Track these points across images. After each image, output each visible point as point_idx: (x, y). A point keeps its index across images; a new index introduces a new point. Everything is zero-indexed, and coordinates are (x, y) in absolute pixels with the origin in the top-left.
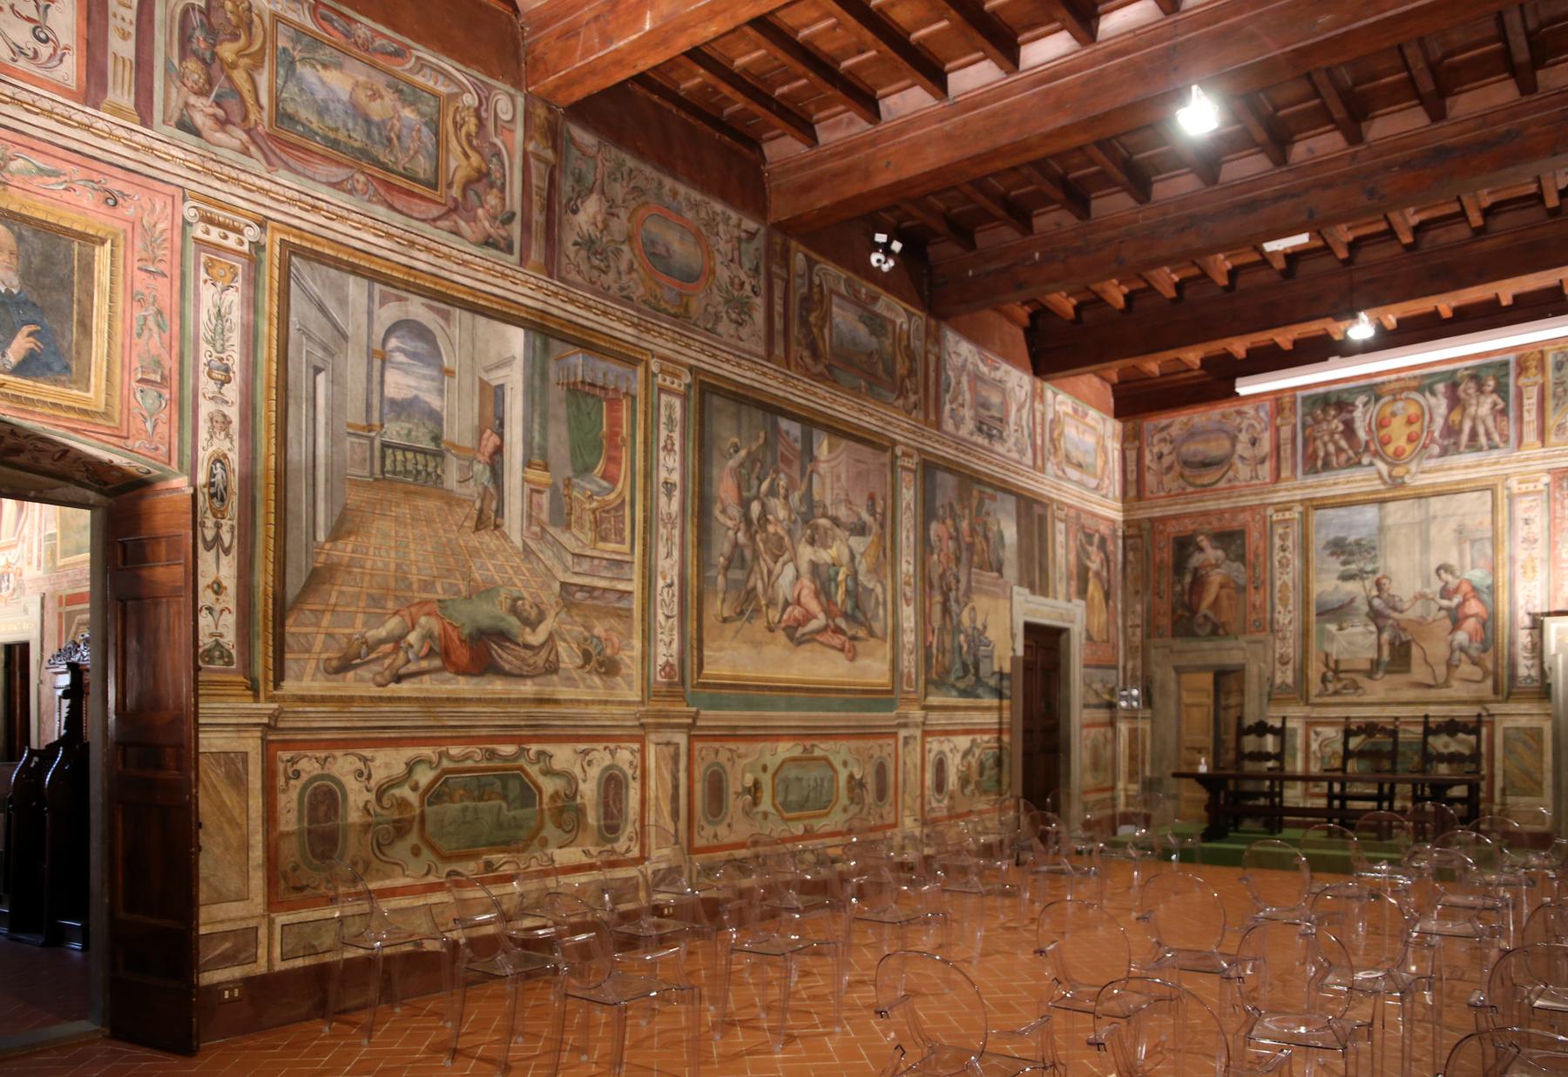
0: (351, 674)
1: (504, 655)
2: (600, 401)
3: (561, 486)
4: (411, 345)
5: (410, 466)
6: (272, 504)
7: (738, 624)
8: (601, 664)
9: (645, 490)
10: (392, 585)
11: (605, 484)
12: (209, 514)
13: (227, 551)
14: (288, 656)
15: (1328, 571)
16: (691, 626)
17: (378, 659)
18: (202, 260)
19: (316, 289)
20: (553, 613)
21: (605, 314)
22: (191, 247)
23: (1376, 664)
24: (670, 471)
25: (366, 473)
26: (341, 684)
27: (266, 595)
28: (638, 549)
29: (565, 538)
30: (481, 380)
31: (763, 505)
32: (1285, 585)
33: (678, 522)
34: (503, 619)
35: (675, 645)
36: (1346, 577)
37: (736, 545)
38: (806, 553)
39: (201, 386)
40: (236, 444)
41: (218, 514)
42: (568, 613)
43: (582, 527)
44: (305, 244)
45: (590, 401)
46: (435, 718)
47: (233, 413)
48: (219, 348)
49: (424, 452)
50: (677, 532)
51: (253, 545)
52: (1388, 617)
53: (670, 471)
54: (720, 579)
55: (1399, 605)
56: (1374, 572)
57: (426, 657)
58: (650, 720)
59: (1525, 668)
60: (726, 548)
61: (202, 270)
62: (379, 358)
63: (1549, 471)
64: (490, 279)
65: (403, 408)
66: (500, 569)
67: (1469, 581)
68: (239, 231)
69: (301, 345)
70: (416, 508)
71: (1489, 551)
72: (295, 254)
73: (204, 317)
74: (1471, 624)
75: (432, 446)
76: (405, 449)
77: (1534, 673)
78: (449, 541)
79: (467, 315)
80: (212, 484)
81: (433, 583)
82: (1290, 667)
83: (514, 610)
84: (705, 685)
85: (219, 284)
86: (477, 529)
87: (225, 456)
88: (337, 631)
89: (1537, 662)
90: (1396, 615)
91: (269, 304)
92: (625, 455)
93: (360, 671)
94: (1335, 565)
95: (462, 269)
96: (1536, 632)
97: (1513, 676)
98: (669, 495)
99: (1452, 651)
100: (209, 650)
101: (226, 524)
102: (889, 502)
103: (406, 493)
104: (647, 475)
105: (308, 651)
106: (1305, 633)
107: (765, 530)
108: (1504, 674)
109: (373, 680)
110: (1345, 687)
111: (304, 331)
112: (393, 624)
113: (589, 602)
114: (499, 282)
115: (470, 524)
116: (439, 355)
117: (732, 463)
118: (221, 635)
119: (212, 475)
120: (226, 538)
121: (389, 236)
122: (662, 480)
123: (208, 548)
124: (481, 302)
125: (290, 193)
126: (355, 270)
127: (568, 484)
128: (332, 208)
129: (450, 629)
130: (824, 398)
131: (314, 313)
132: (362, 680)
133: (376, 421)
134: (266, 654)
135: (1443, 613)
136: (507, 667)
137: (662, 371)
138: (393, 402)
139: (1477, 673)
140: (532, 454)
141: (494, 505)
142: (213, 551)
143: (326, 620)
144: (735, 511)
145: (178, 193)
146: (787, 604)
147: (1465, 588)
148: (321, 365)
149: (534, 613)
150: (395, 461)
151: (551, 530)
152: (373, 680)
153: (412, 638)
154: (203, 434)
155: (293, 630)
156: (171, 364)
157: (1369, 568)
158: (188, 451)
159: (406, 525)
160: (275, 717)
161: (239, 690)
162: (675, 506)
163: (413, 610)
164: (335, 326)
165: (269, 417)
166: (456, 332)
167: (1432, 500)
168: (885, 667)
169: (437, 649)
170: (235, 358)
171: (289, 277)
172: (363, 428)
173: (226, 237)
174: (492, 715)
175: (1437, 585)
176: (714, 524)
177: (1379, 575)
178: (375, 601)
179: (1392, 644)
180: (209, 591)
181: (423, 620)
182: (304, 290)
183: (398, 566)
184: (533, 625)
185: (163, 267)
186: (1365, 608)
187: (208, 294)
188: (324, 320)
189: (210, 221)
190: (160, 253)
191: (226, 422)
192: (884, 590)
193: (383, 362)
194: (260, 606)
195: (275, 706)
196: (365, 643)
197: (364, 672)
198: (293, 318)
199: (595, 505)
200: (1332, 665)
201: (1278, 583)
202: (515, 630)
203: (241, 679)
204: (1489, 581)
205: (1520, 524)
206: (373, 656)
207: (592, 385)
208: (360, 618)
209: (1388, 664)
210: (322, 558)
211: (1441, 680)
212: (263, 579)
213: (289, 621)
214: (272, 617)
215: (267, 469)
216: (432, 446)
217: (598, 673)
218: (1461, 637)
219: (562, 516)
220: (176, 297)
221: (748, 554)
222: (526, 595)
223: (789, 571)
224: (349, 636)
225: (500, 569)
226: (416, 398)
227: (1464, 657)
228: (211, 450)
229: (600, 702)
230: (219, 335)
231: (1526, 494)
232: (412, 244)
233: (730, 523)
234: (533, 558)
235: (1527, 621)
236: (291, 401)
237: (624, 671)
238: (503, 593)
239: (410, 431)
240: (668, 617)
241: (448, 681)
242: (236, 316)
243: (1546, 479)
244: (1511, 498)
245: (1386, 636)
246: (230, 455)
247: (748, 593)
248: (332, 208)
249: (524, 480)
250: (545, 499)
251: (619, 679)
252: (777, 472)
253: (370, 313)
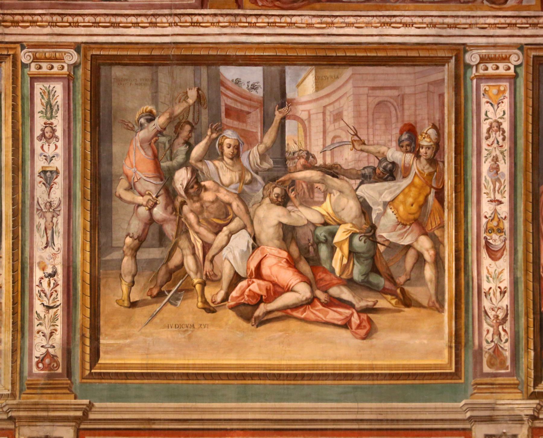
7: (157, 307)
9: (15, 183)
16: (83, 316)
31: (195, 171)
33: (63, 210)
35: (58, 337)
37: (151, 221)
38: (270, 217)
54: (127, 263)
58: (21, 414)
60: (136, 227)
84: (101, 376)
98: (49, 184)
102: (449, 128)
107: (200, 199)
117: (142, 134)
122: (38, 169)
130: (310, 26)
137: (35, 59)
144: (150, 185)
146: (237, 278)
162: (58, 192)
168: (443, 341)
176: (116, 204)
192: (437, 244)
221: (170, 229)
223: (242, 241)
233: (140, 200)
247: (170, 273)
252: (220, 130)
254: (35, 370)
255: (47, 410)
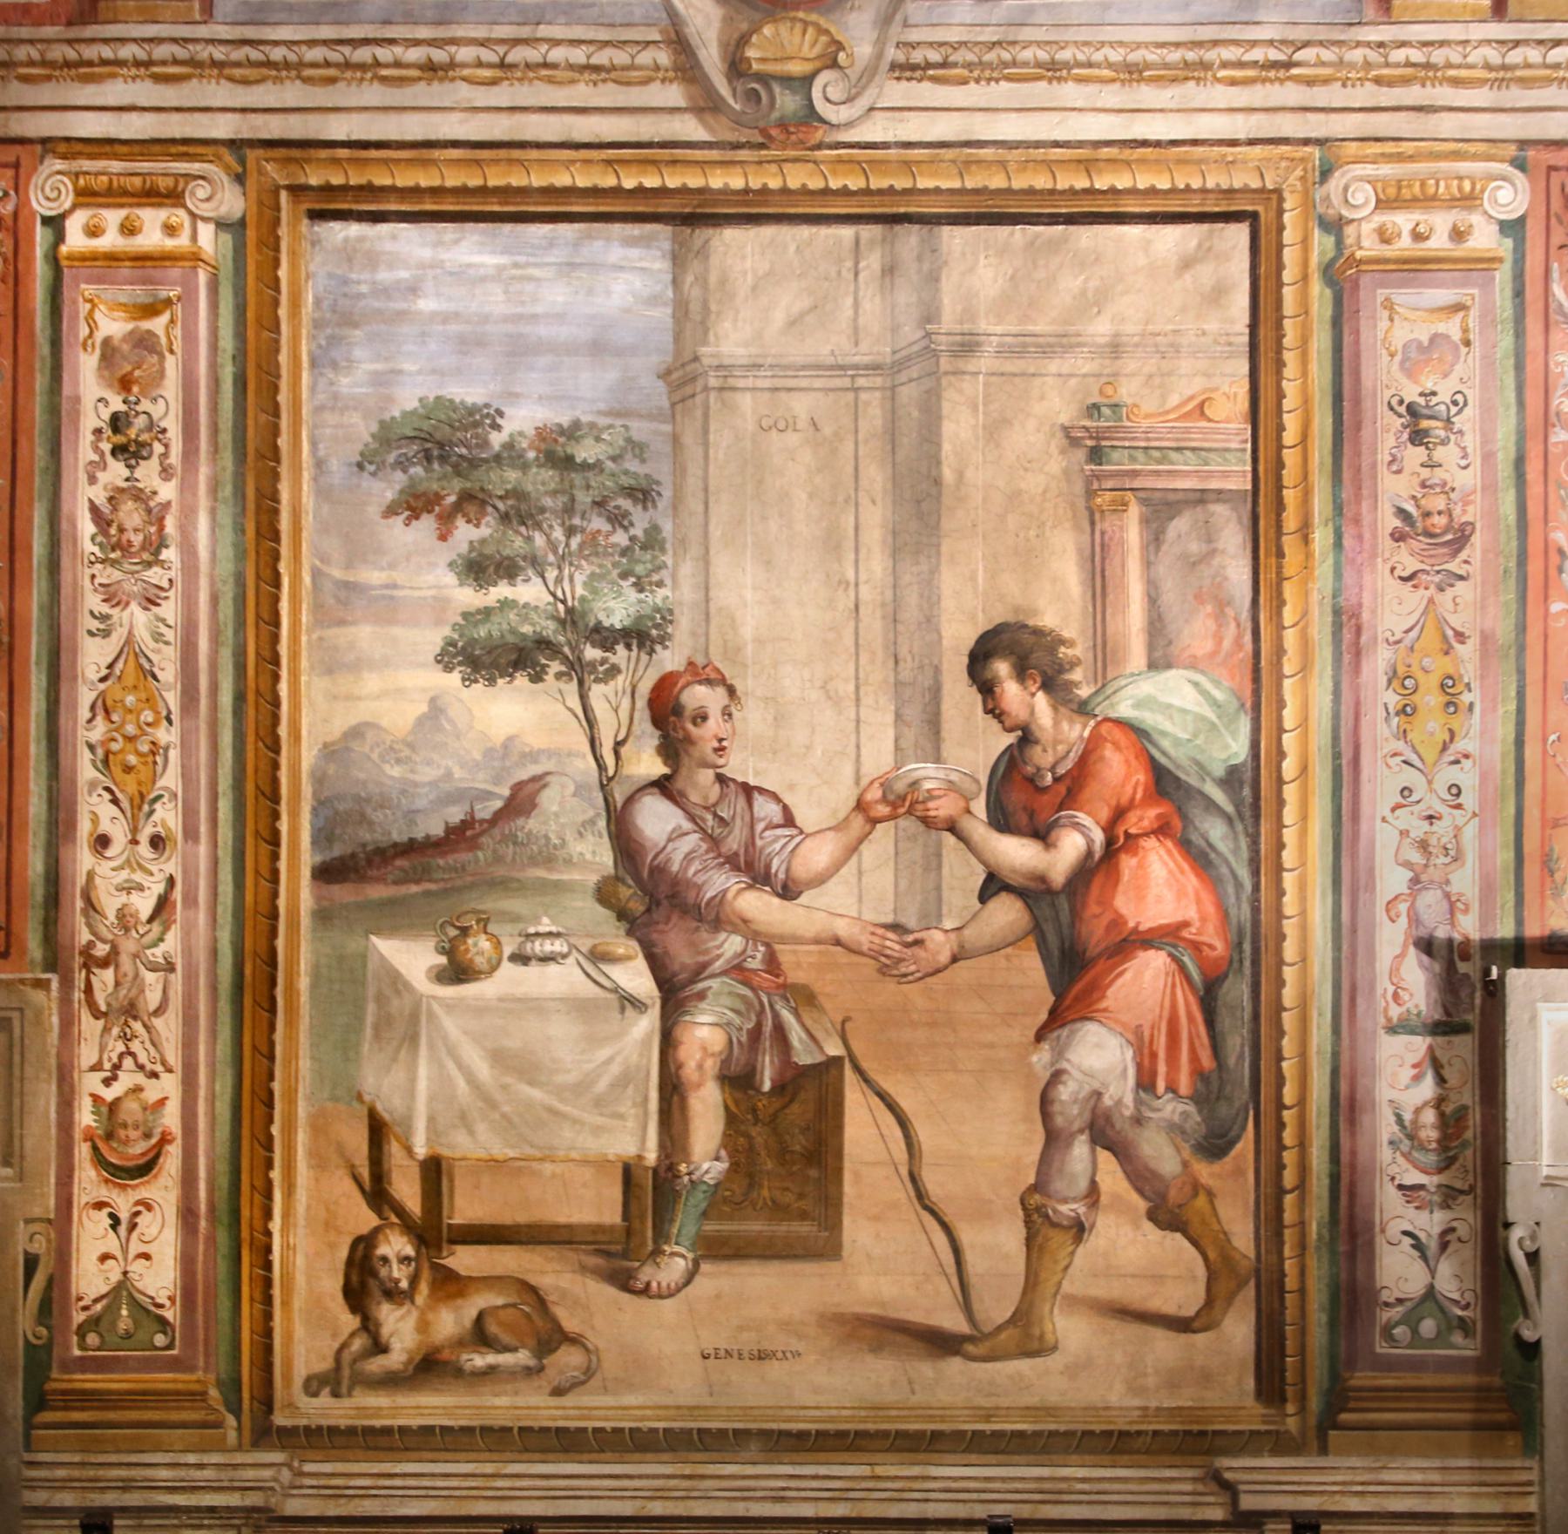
15: (387, 608)
23: (652, 1192)
32: (133, 667)
36: (490, 657)
52: (716, 917)
55: (774, 844)
56: (641, 636)
59: (1412, 1257)
63: (1522, 154)
67: (1137, 732)
71: (1238, 573)
74: (1146, 982)
77: (1453, 1279)
82: (163, 1190)
89: (1466, 1219)
90: (757, 905)
94: (423, 572)
96: (1464, 1047)
97: (1353, 1297)
99: (1054, 1139)
106: (253, 988)
108: (1311, 1279)
110: (480, 1336)
135: (1007, 913)
137: (87, 196)
139: (1165, 1267)
147: (1119, 771)
157: (617, 609)
167: (955, 238)
175: (975, 747)
177: (670, 659)
179: (738, 1080)
186: (598, 855)
200: (407, 1190)
201: (93, 656)
204: (1237, 748)
205: (1387, 432)
209: (720, 1200)
211: (996, 1307)
218: (1099, 1057)
227: (1108, 1167)
231: (1416, 268)
235: (1415, 987)
243: (1511, 196)
244: (1343, 280)
245: (705, 1033)
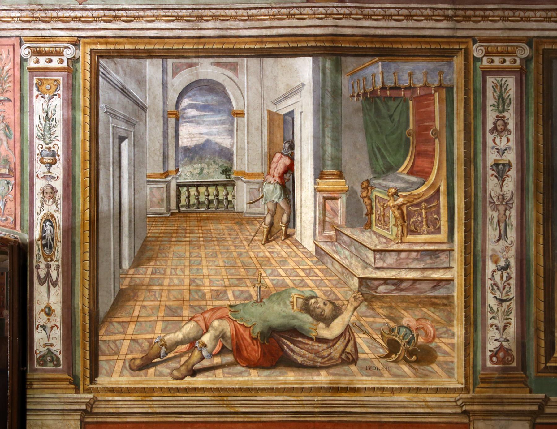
0: (151, 371)
1: (297, 349)
2: (406, 101)
3: (358, 189)
4: (201, 100)
5: (202, 198)
6: (87, 245)
8: (411, 353)
10: (187, 296)
11: (413, 179)
12: (42, 259)
13: (55, 284)
14: (101, 358)
16: (536, 309)
17: (175, 357)
18: (35, 82)
19: (118, 78)
20: (350, 308)
21: (409, 17)
22: (27, 75)
24: (501, 152)
25: (164, 210)
26: (144, 378)
27: (84, 313)
28: (459, 236)
29: (366, 237)
30: (270, 112)
34: (295, 317)
35: (512, 330)
39: (35, 170)
40: (60, 206)
41: (48, 258)
42: (370, 306)
43: (385, 224)
44: (109, 47)
45: (392, 104)
46: (228, 406)
47: (58, 185)
48: (47, 141)
49: (215, 184)
50: (513, 213)
51: (73, 278)
53: (501, 152)
57: (219, 354)
58: (476, 408)
61: (35, 89)
62: (176, 116)
64: (276, 23)
65: (194, 153)
66: (292, 273)
68: (60, 54)
69: (108, 123)
70: (209, 232)
72: (102, 57)
73: (36, 122)
75: (223, 178)
76: (197, 185)
78: (240, 254)
79: (254, 62)
80: (43, 238)
81: (225, 292)
83: (306, 308)
85: (47, 96)
86: (267, 241)
87: (53, 216)
88: (140, 337)
91: (83, 100)
92: (439, 148)
93: (160, 368)
95: (248, 24)
100: (43, 356)
101: (54, 264)
103: (199, 220)
104: (470, 161)
105: (117, 353)
109: (171, 374)
111: (111, 113)
112: (188, 329)
113: (396, 294)
114: (286, 23)
115: (261, 237)
116: (229, 101)
118: (52, 345)
119: (44, 231)
120: (54, 275)
121: (179, 18)
123: (42, 283)
124: (268, 46)
125: (96, 13)
126: (150, 54)
127: (367, 186)
128: (129, 13)
129: (241, 329)
131: (118, 97)
132: (161, 375)
133: (171, 167)
134: (84, 357)
136: (300, 360)
138: (187, 149)
140: (324, 165)
141: (285, 218)
142: (45, 285)
143: (131, 329)
145: (17, 41)
148: (124, 134)
149: (328, 310)
150: (189, 197)
151: (348, 232)
152: (171, 374)
153: (206, 338)
154: (37, 203)
155: (105, 338)
156: (15, 159)
158: (27, 217)
159: (199, 247)
160: (91, 404)
161: (64, 384)
163: (207, 315)
164: (136, 102)
165: (84, 183)
166: (243, 78)
169: (229, 347)
170: (59, 145)
171: (98, 75)
172: (161, 175)
173: (51, 61)
174: (284, 403)
178: (172, 311)
180: (43, 314)
181: (216, 323)
182: (109, 81)
183: (192, 281)
184: (328, 321)
185: (8, 95)
187: (39, 105)
188: (126, 100)
189: (39, 53)
190: (6, 86)
191: (54, 191)
193: (177, 119)
194: (79, 322)
195: (91, 396)
196: (165, 345)
197: (163, 369)
198: (102, 105)
199: (401, 200)
202: (307, 327)
203: (66, 376)
206: (171, 355)
207: (396, 88)
208: (160, 326)
210: (127, 281)
212: (81, 302)
213: (102, 332)
214: (88, 332)
215: (84, 220)
216: (223, 178)
217: (408, 362)
219: (361, 214)
220: (18, 113)
222: (318, 293)
224: (150, 341)
225: (292, 273)
226: (208, 141)
228: (42, 214)
229: (409, 390)
230: (48, 130)
232: (200, 18)
234: (327, 259)
236: (101, 167)
237: (441, 358)
238: (294, 294)
239: (202, 170)
240: (501, 301)
241: (240, 374)
242: (59, 115)
246: (56, 215)
248: (129, 13)
249: (316, 190)
250: (340, 204)
251: (434, 366)
253: (165, 85)
254: (489, 364)
255: (502, 404)
